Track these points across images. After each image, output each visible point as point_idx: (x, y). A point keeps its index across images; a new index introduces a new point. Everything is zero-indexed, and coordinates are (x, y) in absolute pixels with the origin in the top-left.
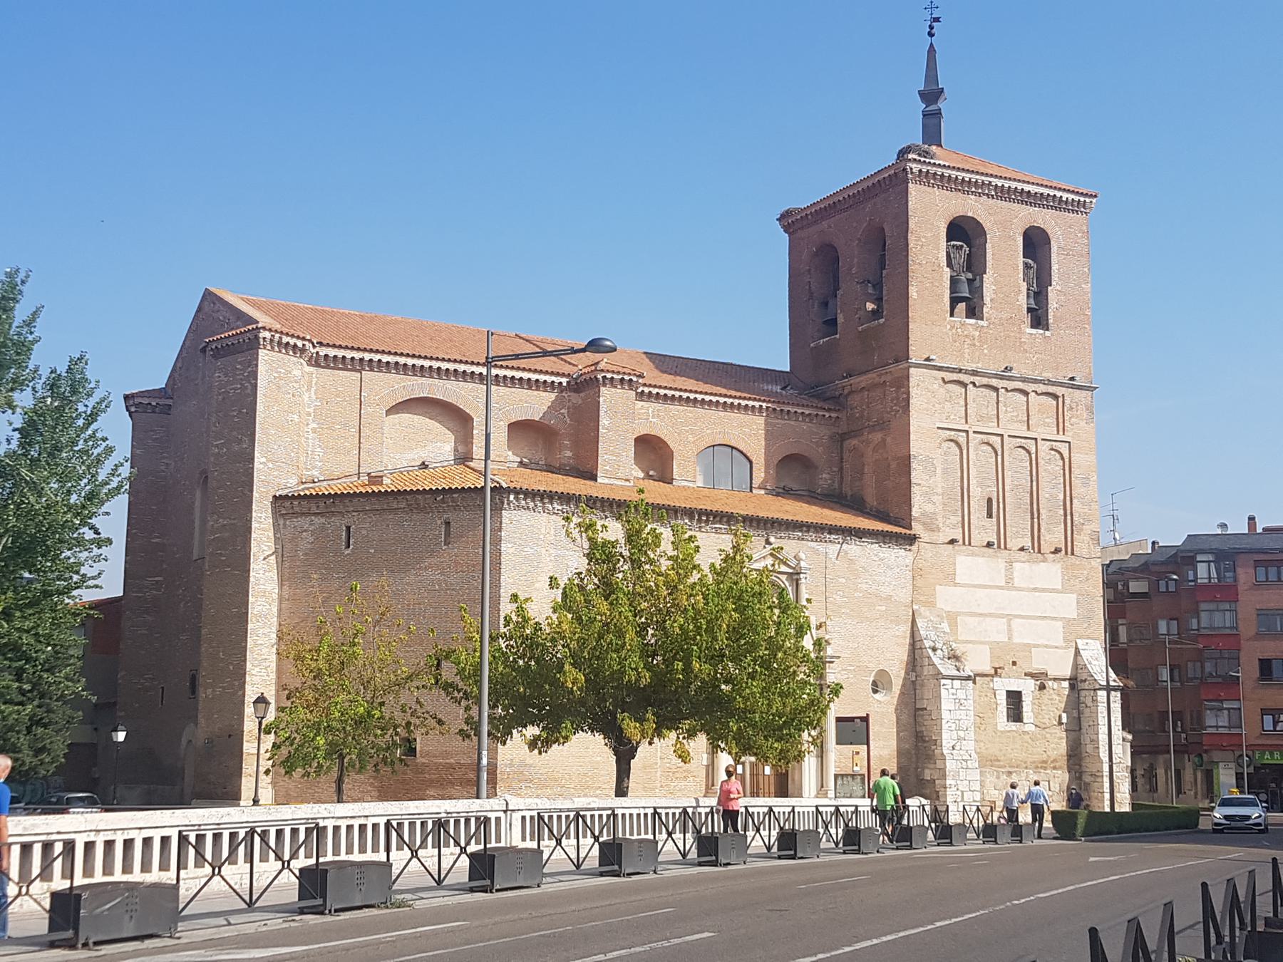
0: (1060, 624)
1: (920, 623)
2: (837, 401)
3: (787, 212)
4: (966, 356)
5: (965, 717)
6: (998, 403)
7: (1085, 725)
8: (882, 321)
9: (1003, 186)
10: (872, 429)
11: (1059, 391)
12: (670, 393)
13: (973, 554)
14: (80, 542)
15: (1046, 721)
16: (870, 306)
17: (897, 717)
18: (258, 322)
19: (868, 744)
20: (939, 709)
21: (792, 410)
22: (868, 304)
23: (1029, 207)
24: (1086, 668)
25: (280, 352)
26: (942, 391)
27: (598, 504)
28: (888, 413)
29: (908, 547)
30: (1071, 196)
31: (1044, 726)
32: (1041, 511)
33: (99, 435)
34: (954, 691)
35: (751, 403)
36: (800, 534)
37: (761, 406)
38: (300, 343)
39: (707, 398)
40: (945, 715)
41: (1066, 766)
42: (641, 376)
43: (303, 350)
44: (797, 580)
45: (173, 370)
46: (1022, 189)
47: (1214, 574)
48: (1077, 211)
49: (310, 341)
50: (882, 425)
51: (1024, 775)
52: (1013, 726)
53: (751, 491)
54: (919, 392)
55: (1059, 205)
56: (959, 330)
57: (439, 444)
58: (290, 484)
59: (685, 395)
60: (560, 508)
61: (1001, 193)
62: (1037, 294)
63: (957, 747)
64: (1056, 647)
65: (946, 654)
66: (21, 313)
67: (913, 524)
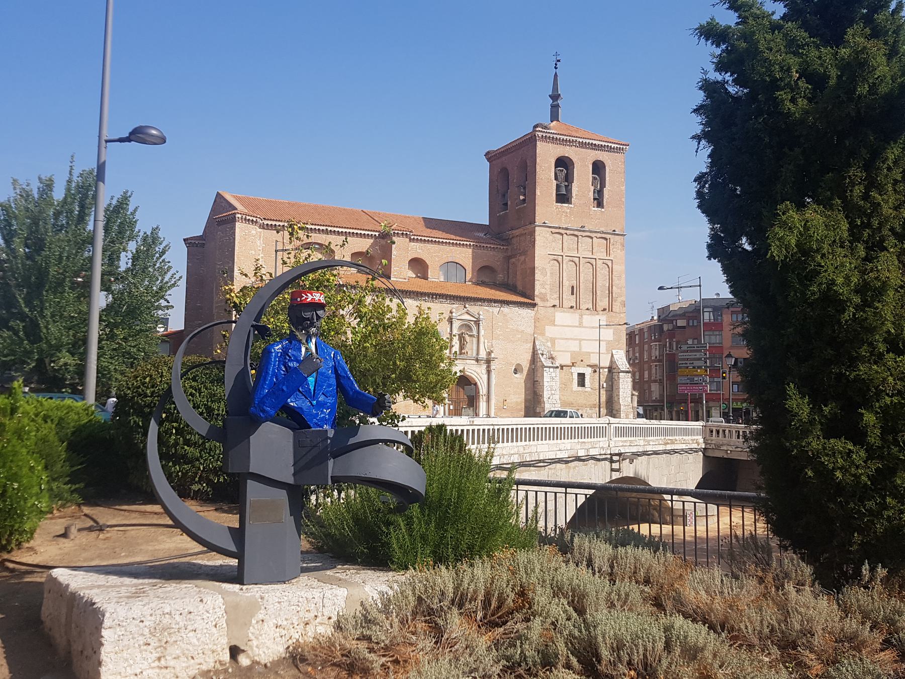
1: (537, 343)
2: (507, 241)
7: (614, 388)
8: (525, 205)
10: (521, 254)
11: (608, 236)
12: (427, 239)
13: (564, 311)
16: (522, 197)
18: (237, 209)
26: (551, 237)
30: (616, 146)
32: (597, 292)
33: (166, 260)
35: (465, 243)
38: (255, 219)
40: (546, 384)
43: (256, 222)
44: (479, 324)
47: (712, 318)
50: (524, 253)
51: (584, 411)
52: (580, 389)
55: (610, 150)
59: (434, 239)
62: (599, 192)
66: (131, 208)
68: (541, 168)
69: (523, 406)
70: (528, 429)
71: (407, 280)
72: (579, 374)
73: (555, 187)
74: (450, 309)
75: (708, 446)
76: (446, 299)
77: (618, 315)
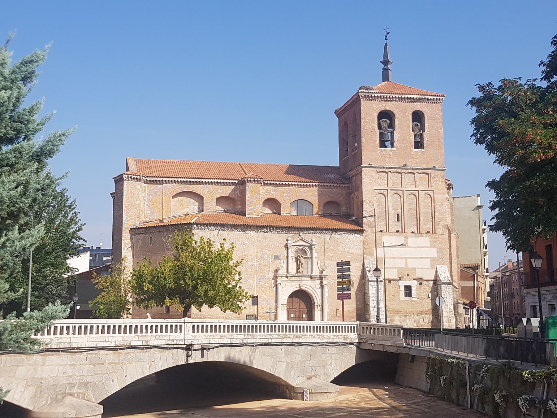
0: (429, 260)
3: (336, 110)
4: (387, 162)
6: (401, 178)
9: (401, 97)
12: (278, 183)
13: (390, 235)
15: (423, 297)
19: (258, 305)
21: (329, 185)
25: (132, 181)
26: (377, 175)
27: (229, 226)
29: (361, 234)
30: (432, 97)
31: (421, 298)
32: (420, 218)
35: (311, 184)
36: (313, 232)
38: (138, 177)
41: (431, 313)
43: (140, 179)
44: (312, 248)
46: (410, 97)
49: (142, 176)
52: (407, 298)
54: (366, 177)
56: (384, 152)
57: (193, 207)
58: (137, 224)
60: (214, 228)
64: (427, 269)
67: (364, 225)
68: (365, 120)
69: (355, 314)
70: (164, 327)
71: (259, 216)
72: (406, 287)
73: (378, 135)
74: (286, 238)
75: (361, 341)
76: (282, 229)
77: (441, 236)
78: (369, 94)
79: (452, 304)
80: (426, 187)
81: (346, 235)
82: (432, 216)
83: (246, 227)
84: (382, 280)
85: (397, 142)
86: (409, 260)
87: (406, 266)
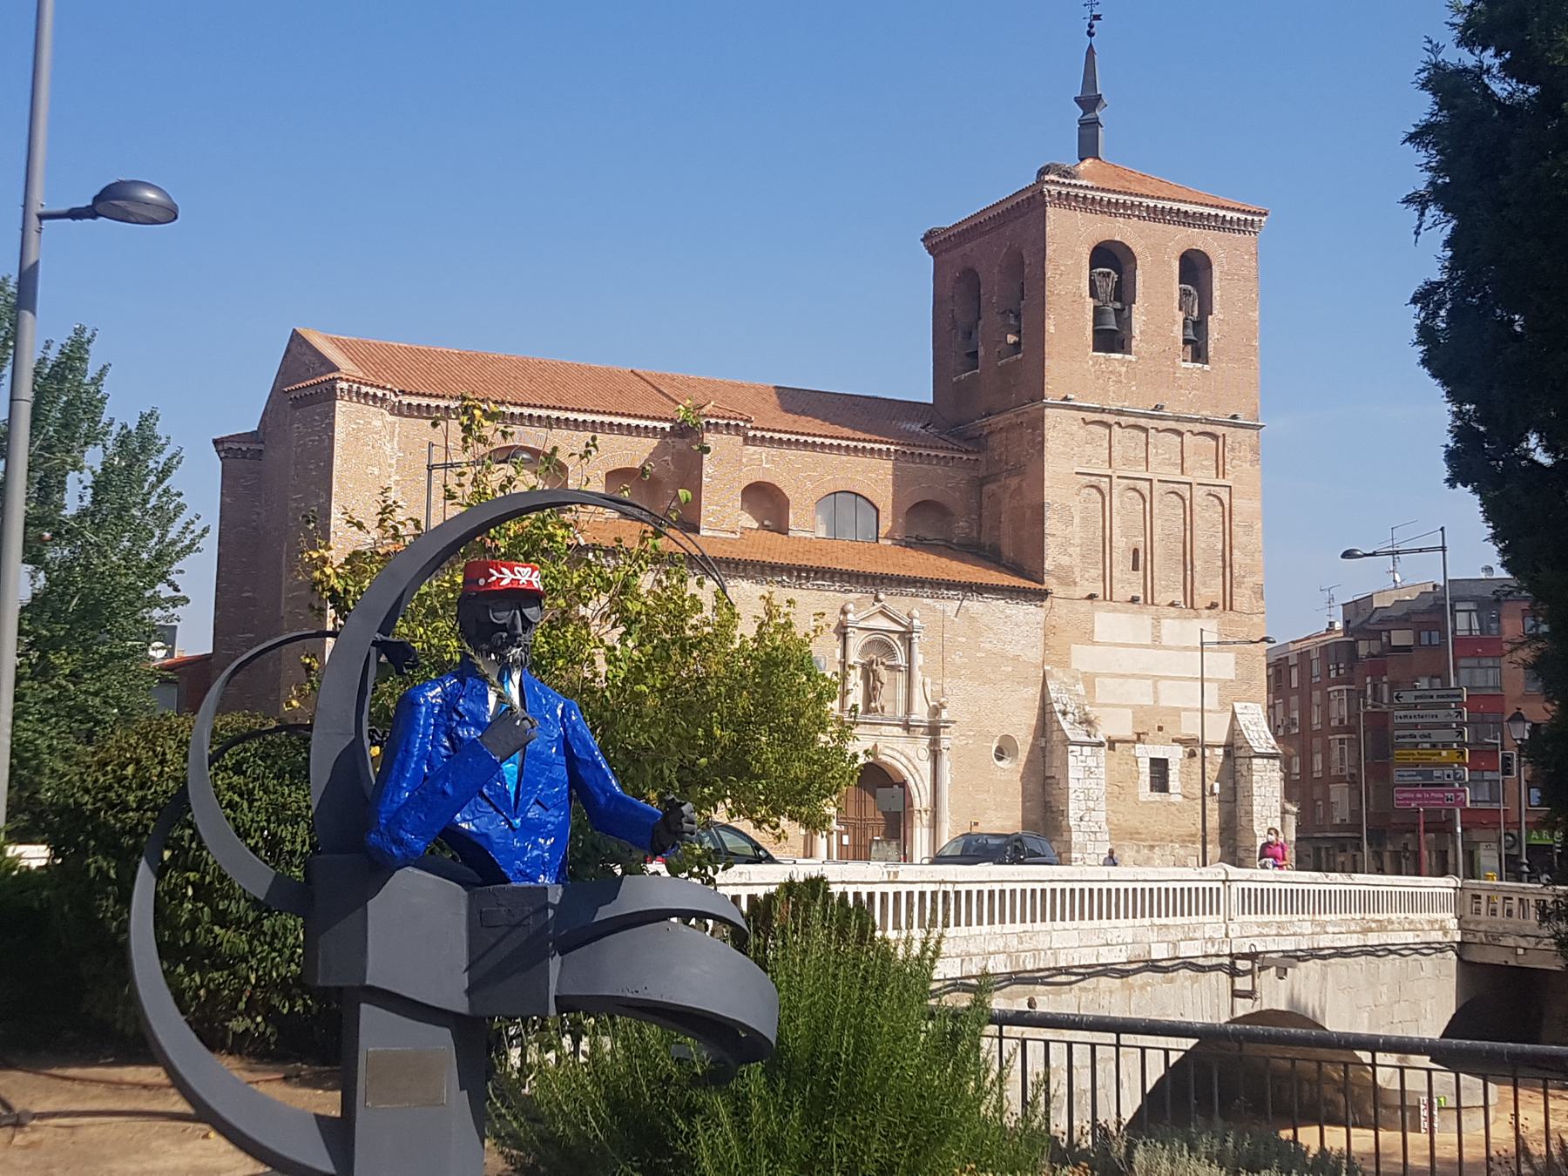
1: (1051, 686)
5: (1095, 787)
6: (1147, 444)
8: (1020, 356)
10: (1010, 473)
11: (1219, 430)
12: (785, 437)
13: (1115, 610)
14: (155, 602)
16: (1011, 339)
17: (1023, 787)
20: (1067, 778)
21: (925, 453)
22: (1009, 336)
23: (1186, 228)
24: (1243, 734)
25: (359, 402)
26: (1081, 433)
28: (1025, 456)
29: (1039, 603)
30: (1236, 215)
32: (1195, 563)
34: (1083, 758)
35: (877, 446)
36: (914, 590)
37: (888, 449)
39: (828, 441)
40: (1073, 784)
42: (748, 420)
43: (383, 399)
44: (911, 639)
45: (264, 414)
46: (1179, 209)
47: (1476, 626)
48: (1244, 231)
49: (391, 390)
50: (1018, 470)
52: (1157, 796)
53: (877, 541)
55: (1223, 224)
56: (1103, 366)
61: (1155, 214)
63: (1086, 819)
65: (1077, 718)
66: (92, 370)
72: (1154, 762)
75: (1469, 938)
76: (832, 579)
78: (1070, 189)
79: (1279, 814)
80: (1209, 476)
81: (1000, 605)
82: (1224, 561)
83: (732, 565)
84: (1104, 740)
85: (1139, 338)
86: (1162, 685)
87: (1155, 702)
